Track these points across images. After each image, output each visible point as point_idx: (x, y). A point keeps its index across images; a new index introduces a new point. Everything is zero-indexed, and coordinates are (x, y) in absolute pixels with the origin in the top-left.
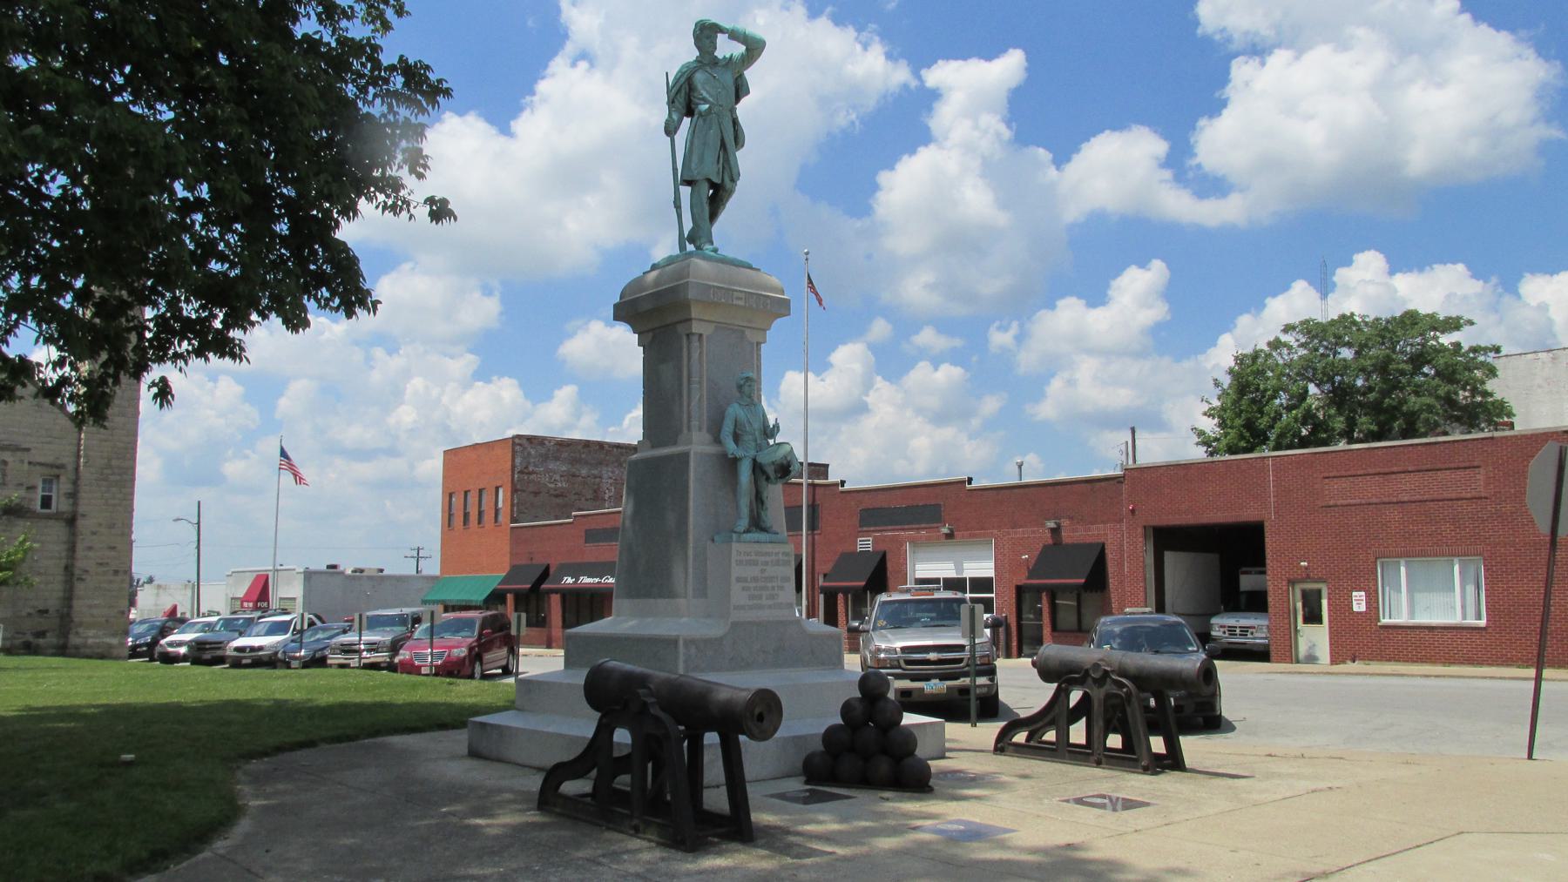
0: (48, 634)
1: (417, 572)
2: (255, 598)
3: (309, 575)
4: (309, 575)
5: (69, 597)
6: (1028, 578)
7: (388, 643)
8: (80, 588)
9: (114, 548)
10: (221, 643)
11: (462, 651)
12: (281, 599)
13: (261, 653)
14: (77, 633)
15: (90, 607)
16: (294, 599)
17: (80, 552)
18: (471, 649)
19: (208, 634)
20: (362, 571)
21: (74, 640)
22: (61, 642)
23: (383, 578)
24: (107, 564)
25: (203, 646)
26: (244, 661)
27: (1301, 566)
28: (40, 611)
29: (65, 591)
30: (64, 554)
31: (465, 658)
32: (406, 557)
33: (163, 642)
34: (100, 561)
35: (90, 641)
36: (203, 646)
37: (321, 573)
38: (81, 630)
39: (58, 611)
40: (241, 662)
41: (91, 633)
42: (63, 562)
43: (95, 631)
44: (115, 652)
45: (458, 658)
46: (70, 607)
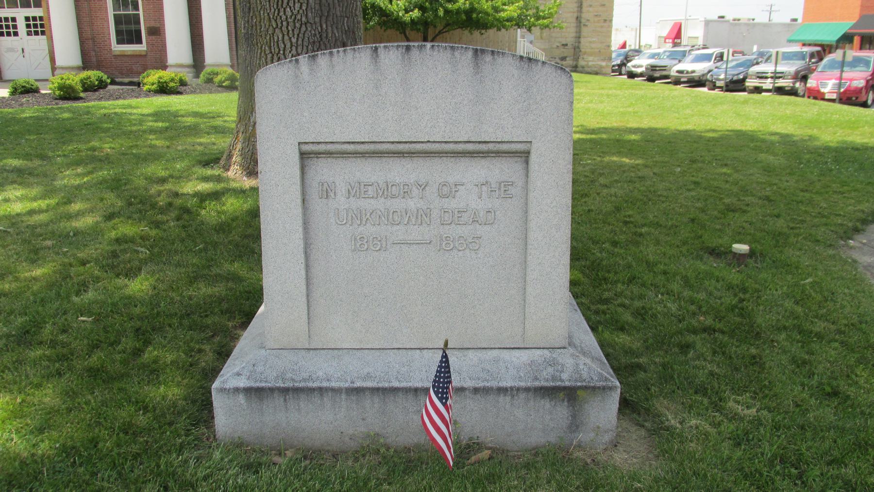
0: (568, 59)
1: (769, 20)
2: (673, 36)
3: (707, 23)
4: (707, 23)
5: (578, 37)
6: (673, 47)
7: (793, 73)
8: (585, 31)
9: (604, 5)
10: (666, 67)
11: (860, 83)
12: (689, 37)
13: (693, 74)
14: (583, 58)
15: (590, 42)
16: (697, 38)
17: (584, 9)
18: (867, 81)
19: (657, 60)
20: (739, 20)
21: (581, 63)
22: (575, 63)
23: (755, 25)
24: (600, 15)
25: (654, 68)
26: (682, 80)
27: (753, 46)
28: (563, 45)
29: (576, 32)
30: (576, 9)
31: (862, 88)
32: (763, 11)
33: (629, 64)
34: (596, 14)
35: (590, 64)
36: (654, 68)
37: (715, 21)
38: (585, 57)
39: (572, 45)
40: (680, 79)
41: (591, 58)
42: (575, 15)
43: (592, 58)
44: (604, 71)
45: (856, 88)
46: (579, 42)
